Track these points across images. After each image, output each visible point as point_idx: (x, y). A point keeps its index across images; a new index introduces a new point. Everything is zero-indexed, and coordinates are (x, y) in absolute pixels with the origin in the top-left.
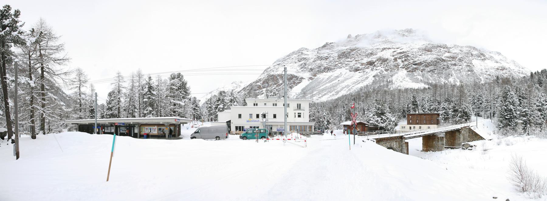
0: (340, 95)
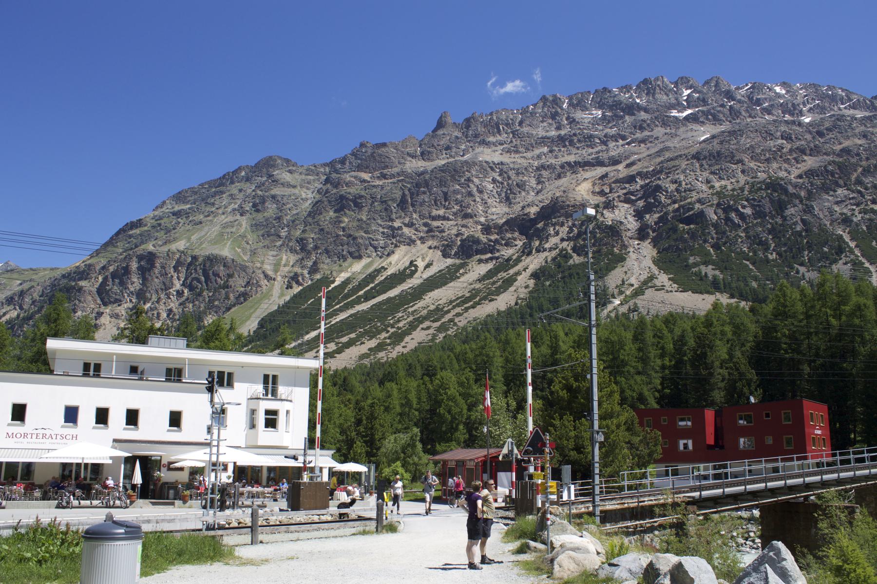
0: (412, 341)
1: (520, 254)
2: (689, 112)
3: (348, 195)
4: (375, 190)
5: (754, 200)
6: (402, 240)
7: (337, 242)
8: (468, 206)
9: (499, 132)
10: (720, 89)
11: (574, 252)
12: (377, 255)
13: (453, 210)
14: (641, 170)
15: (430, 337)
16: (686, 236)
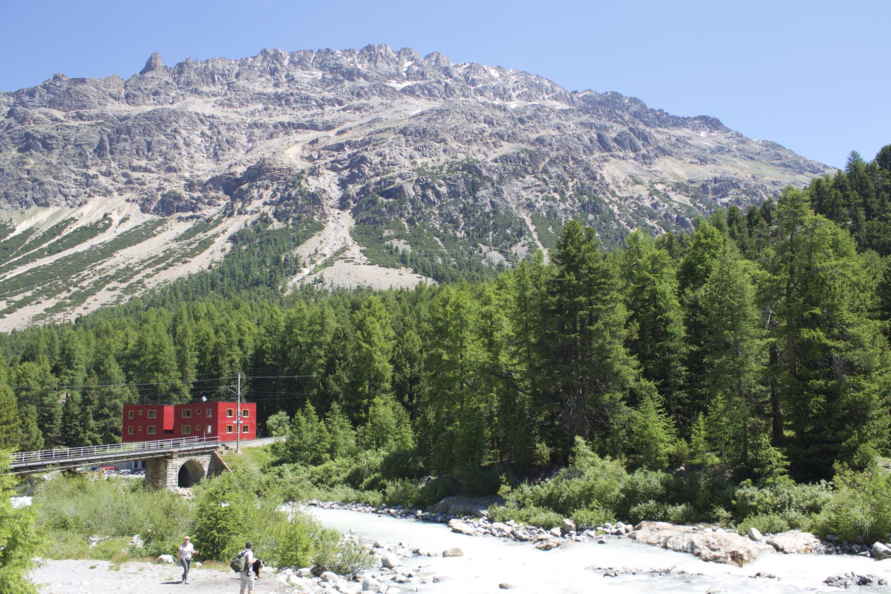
0: (93, 304)
1: (221, 215)
2: (407, 83)
3: (36, 134)
4: (68, 131)
5: (450, 179)
6: (97, 189)
7: (20, 186)
8: (173, 159)
9: (214, 82)
10: (440, 65)
11: (275, 217)
12: (67, 204)
13: (156, 162)
14: (350, 139)
15: (115, 299)
16: (384, 209)
